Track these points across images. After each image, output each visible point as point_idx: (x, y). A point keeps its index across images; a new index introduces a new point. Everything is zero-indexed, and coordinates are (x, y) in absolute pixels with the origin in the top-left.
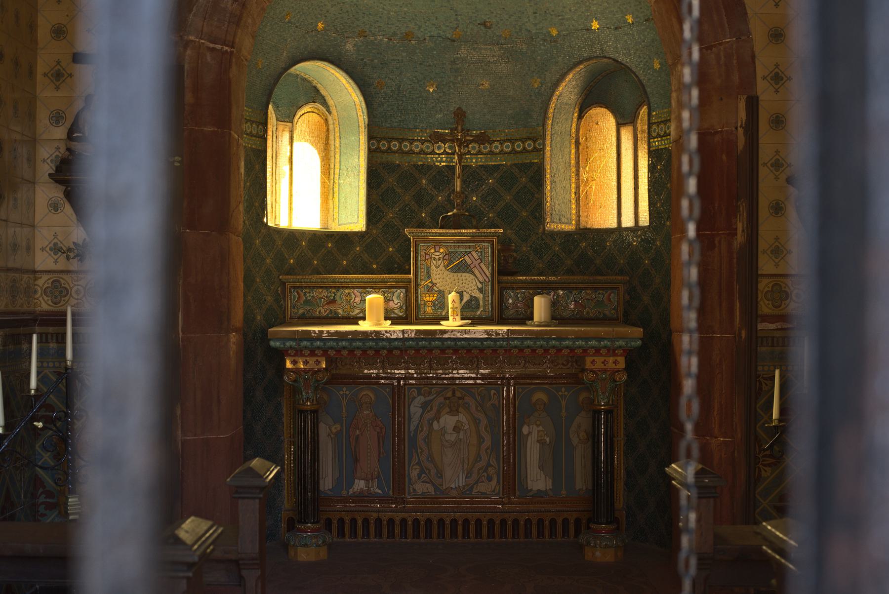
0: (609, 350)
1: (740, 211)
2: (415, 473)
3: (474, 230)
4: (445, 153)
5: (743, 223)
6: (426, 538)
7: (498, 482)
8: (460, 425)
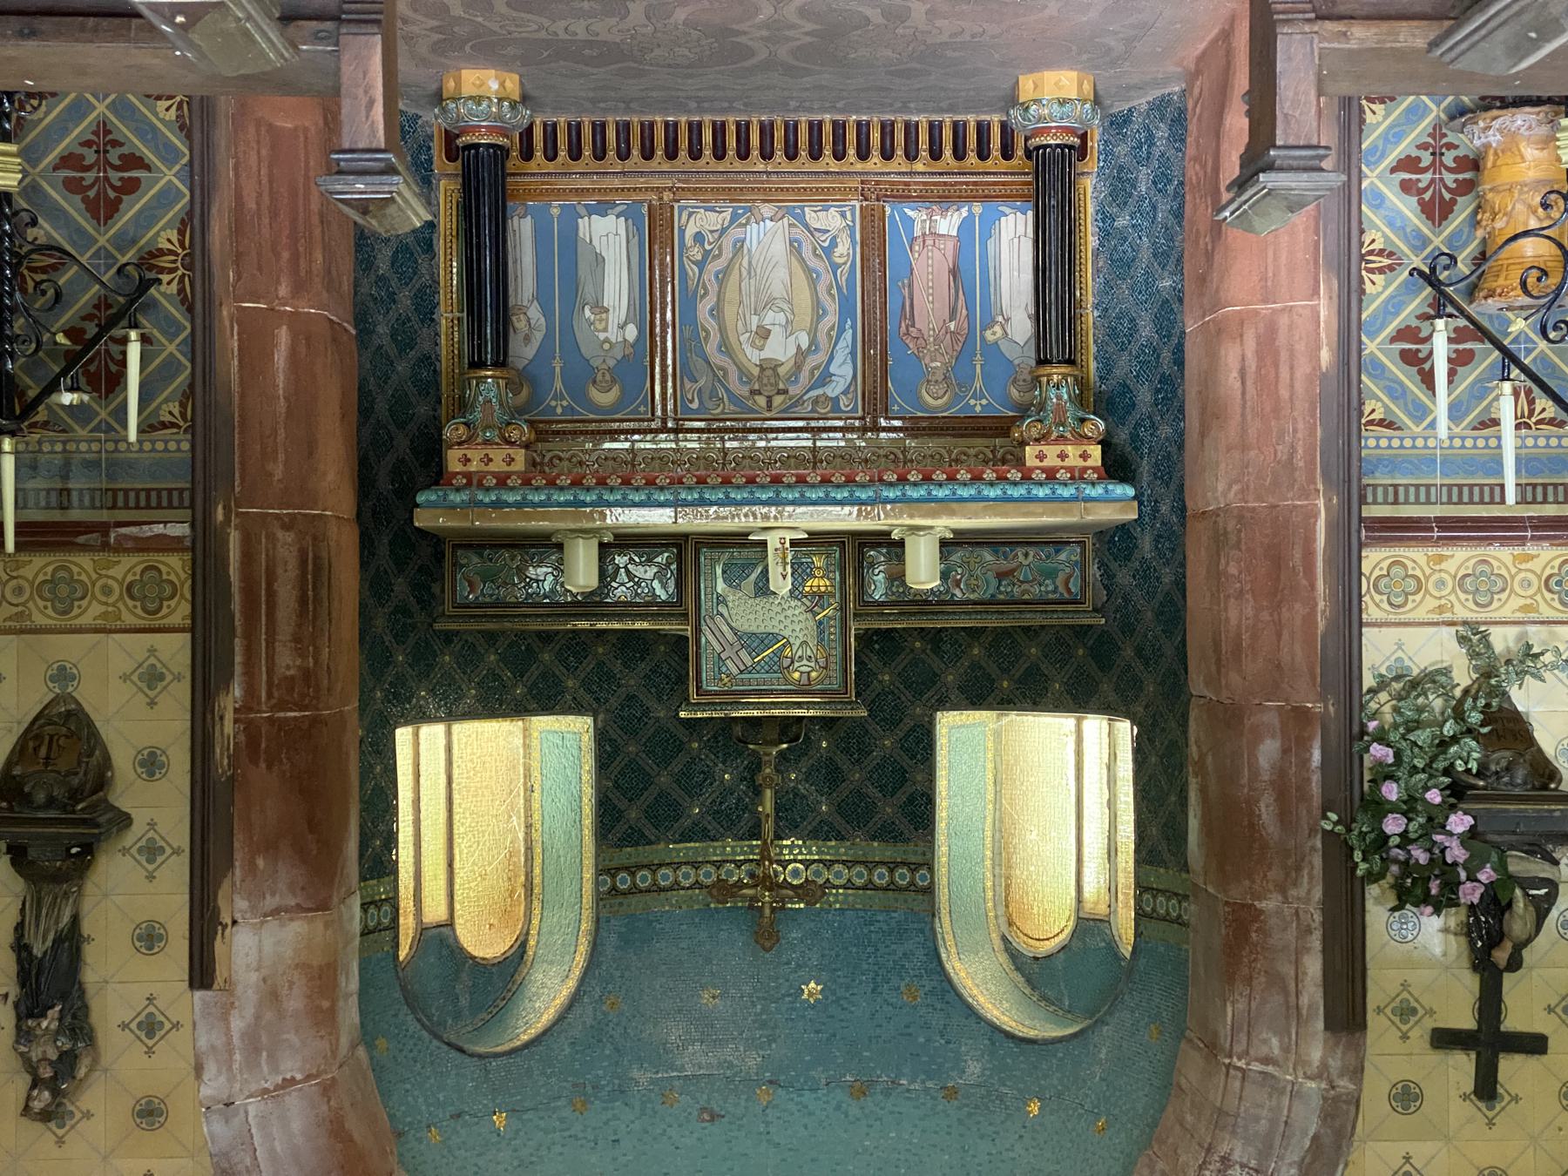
1: (229, 757)
2: (843, 248)
5: (222, 734)
7: (682, 232)
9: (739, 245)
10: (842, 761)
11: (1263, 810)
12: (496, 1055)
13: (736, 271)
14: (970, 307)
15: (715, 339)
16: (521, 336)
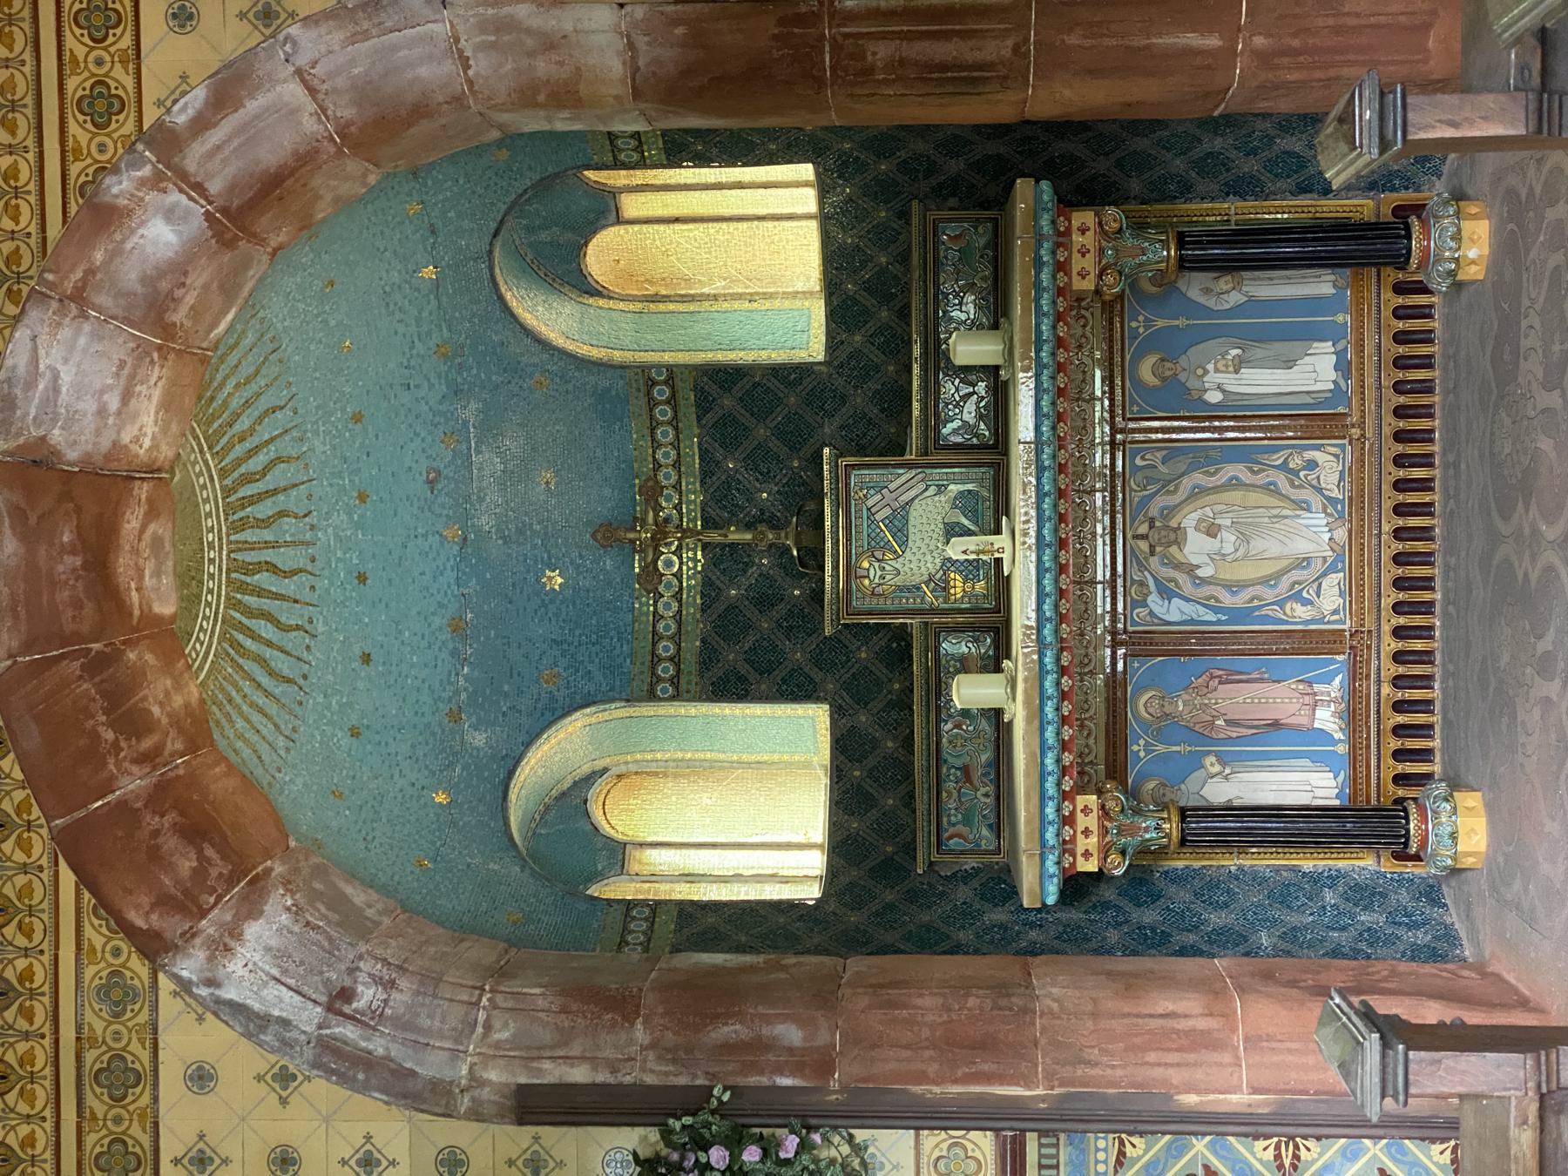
0: (1058, 245)
2: (1301, 612)
4: (674, 423)
6: (1432, 589)
7: (1318, 448)
9: (1305, 506)
10: (781, 610)
11: (732, 1028)
12: (491, 268)
13: (1277, 503)
14: (1239, 740)
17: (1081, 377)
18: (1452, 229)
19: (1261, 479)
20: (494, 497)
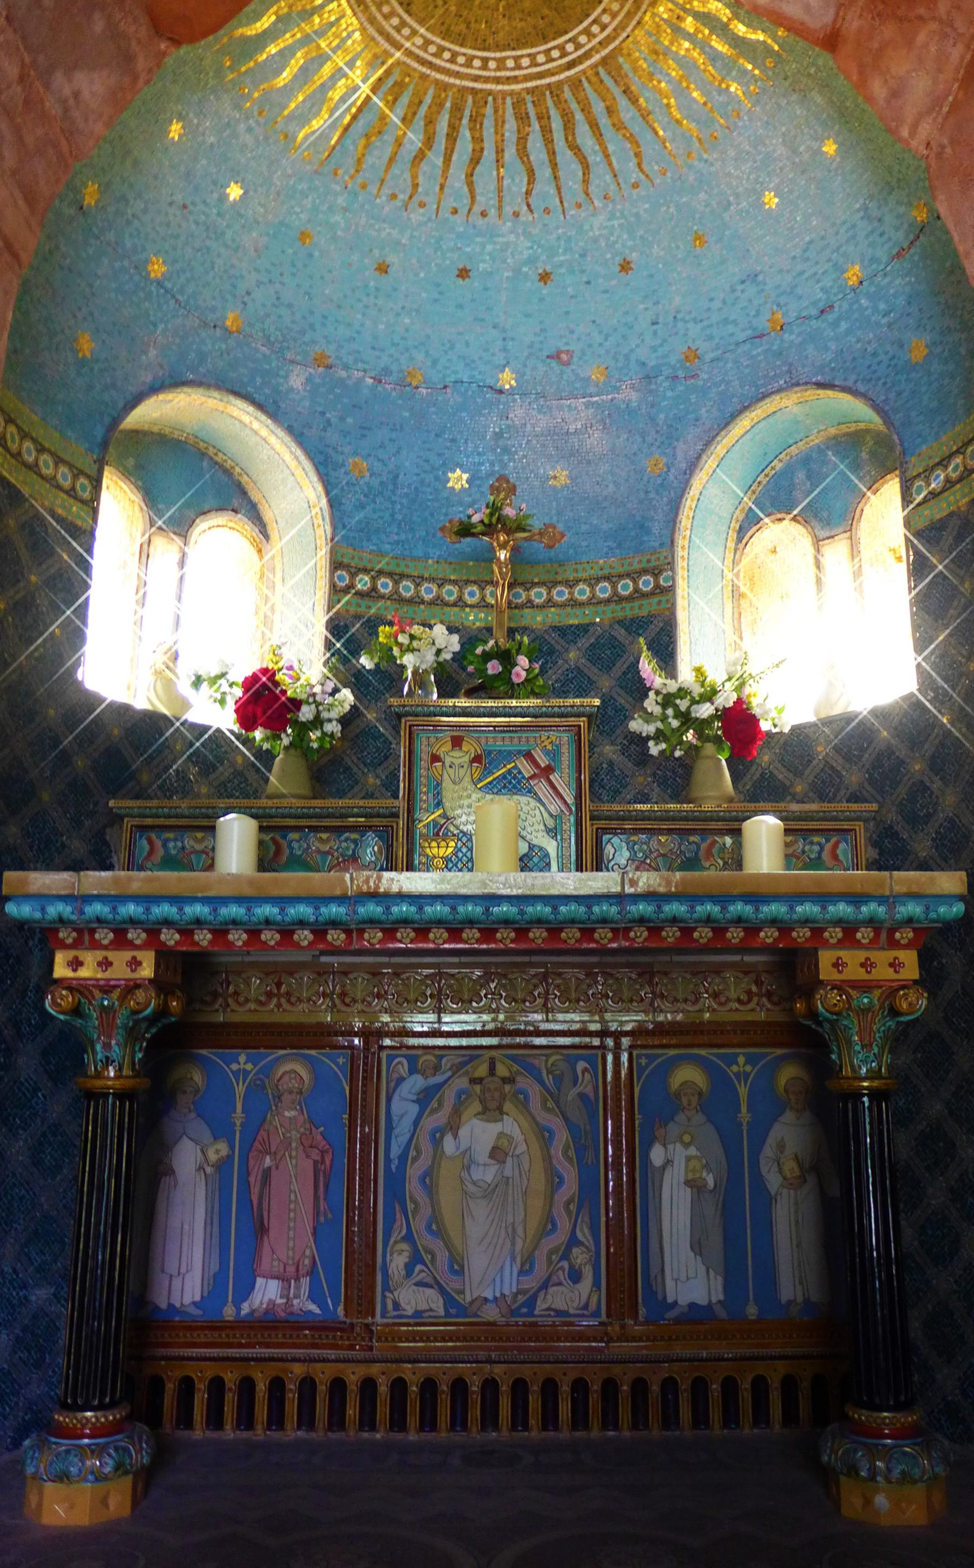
2: (398, 1262)
3: (538, 702)
7: (596, 1284)
8: (506, 1143)
13: (531, 1232)
15: (557, 1150)
16: (789, 1151)
17: (680, 996)
18: (916, 1472)
19: (559, 1211)
20: (543, 422)
